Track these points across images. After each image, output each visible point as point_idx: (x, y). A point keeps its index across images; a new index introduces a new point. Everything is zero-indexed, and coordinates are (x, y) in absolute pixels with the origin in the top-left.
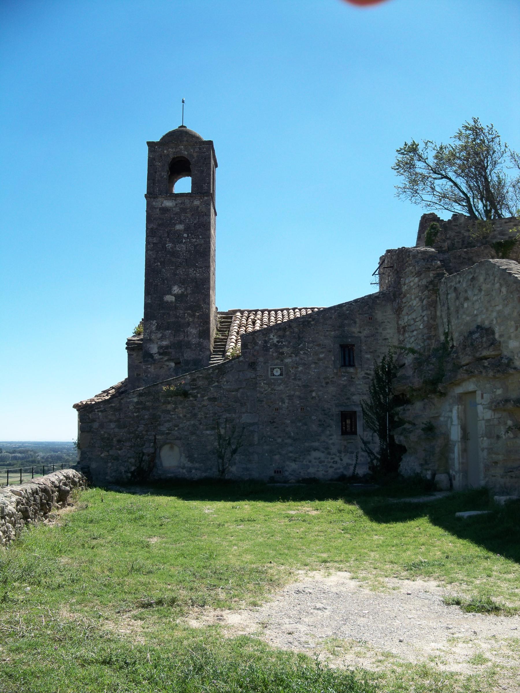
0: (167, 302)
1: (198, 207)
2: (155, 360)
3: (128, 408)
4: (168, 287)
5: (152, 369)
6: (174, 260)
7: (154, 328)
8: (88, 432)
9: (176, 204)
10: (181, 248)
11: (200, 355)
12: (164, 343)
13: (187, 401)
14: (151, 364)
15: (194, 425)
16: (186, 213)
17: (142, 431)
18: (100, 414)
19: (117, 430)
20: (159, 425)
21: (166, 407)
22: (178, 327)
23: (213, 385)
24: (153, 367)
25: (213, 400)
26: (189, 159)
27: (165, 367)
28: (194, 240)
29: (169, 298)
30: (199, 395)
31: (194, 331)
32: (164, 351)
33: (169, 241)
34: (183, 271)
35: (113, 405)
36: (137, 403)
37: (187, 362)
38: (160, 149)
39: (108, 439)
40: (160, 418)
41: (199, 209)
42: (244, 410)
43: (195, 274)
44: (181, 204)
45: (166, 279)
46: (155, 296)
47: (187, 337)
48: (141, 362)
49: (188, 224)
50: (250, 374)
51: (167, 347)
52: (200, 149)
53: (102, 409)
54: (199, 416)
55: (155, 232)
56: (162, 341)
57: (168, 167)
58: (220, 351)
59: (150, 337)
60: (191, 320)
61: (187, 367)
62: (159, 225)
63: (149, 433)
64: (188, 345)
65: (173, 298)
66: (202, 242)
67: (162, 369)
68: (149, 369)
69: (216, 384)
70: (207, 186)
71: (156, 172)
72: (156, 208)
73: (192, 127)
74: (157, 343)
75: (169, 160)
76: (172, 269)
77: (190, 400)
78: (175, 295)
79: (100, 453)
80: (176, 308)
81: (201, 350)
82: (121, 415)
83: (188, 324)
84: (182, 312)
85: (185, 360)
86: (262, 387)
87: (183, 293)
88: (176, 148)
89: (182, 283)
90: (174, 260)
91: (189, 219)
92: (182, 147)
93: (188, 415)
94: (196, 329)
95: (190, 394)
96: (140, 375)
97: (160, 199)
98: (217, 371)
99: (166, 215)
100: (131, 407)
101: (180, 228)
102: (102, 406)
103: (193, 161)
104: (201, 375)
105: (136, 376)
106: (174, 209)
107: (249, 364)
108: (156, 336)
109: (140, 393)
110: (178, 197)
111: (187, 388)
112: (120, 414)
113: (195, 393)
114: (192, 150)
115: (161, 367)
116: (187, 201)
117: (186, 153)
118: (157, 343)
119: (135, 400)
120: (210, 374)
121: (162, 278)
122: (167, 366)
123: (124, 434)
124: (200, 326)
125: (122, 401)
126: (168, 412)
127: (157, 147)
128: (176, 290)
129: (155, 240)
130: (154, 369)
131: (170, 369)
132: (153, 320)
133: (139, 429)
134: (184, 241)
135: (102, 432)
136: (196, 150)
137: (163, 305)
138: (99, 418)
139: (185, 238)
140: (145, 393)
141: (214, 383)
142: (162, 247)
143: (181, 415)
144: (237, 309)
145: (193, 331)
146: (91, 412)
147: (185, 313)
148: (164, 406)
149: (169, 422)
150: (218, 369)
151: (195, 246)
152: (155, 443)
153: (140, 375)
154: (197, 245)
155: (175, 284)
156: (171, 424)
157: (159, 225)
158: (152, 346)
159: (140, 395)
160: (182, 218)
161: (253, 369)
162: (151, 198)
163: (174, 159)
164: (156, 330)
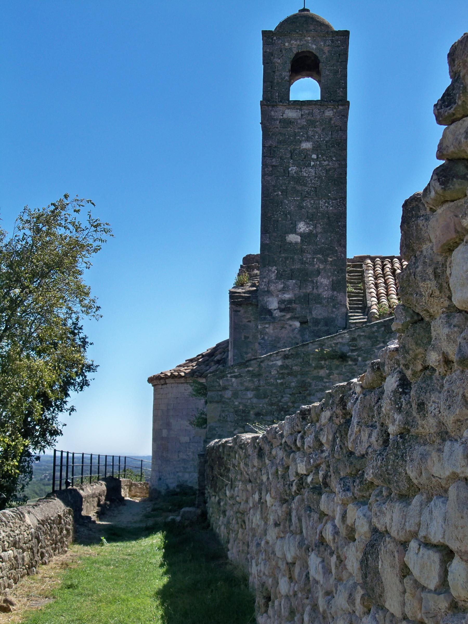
0: (291, 243)
1: (331, 119)
2: (274, 318)
3: (271, 373)
4: (292, 223)
5: (270, 329)
6: (299, 188)
7: (273, 276)
8: (217, 402)
9: (302, 115)
10: (309, 173)
11: (333, 312)
12: (287, 296)
13: (345, 366)
14: (269, 323)
16: (315, 127)
17: (287, 402)
18: (234, 380)
19: (255, 400)
20: (310, 395)
21: (318, 372)
22: (304, 276)
24: (271, 327)
26: (317, 55)
28: (326, 163)
29: (293, 238)
30: (360, 359)
32: (286, 307)
33: (293, 164)
34: (311, 203)
35: (251, 369)
36: (282, 367)
37: (316, 322)
38: (280, 41)
39: (244, 411)
40: (310, 386)
41: (332, 122)
43: (327, 207)
44: (309, 114)
45: (289, 213)
47: (317, 289)
49: (317, 142)
51: (290, 301)
52: (332, 42)
53: (237, 374)
55: (274, 151)
56: (284, 293)
57: (290, 65)
58: (358, 308)
59: (268, 287)
60: (321, 266)
61: (316, 328)
64: (318, 299)
67: (283, 330)
68: (267, 330)
70: (342, 91)
72: (275, 120)
73: (314, 11)
74: (277, 296)
75: (292, 56)
76: (297, 200)
77: (350, 365)
78: (301, 235)
79: (232, 429)
80: (302, 251)
81: (334, 306)
82: (261, 382)
83: (318, 272)
85: (313, 318)
87: (311, 232)
90: (299, 188)
91: (319, 136)
92: (309, 38)
94: (328, 278)
95: (349, 357)
96: (248, 337)
97: (280, 108)
98: (383, 329)
99: (289, 129)
100: (274, 372)
101: (307, 147)
102: (236, 370)
103: (323, 58)
104: (363, 334)
105: (243, 339)
106: (299, 121)
108: (276, 287)
109: (285, 355)
111: (345, 349)
112: (259, 381)
113: (355, 356)
114: (322, 43)
115: (282, 328)
116: (316, 111)
117: (314, 47)
118: (277, 296)
119: (279, 363)
120: (374, 333)
121: (283, 212)
122: (291, 326)
123: (265, 405)
124: (333, 274)
125: (262, 365)
126: (321, 379)
127: (275, 38)
128: (302, 227)
130: (273, 330)
131: (293, 330)
133: (283, 400)
134: (312, 163)
135: (237, 403)
138: (232, 385)
139: (313, 160)
140: (292, 354)
141: (379, 344)
142: (284, 170)
144: (366, 255)
145: (324, 281)
146: (222, 378)
147: (314, 258)
148: (315, 372)
150: (385, 326)
153: (248, 337)
154: (330, 170)
155: (301, 220)
158: (270, 299)
159: (286, 357)
160: (310, 133)
163: (298, 54)
164: (276, 279)
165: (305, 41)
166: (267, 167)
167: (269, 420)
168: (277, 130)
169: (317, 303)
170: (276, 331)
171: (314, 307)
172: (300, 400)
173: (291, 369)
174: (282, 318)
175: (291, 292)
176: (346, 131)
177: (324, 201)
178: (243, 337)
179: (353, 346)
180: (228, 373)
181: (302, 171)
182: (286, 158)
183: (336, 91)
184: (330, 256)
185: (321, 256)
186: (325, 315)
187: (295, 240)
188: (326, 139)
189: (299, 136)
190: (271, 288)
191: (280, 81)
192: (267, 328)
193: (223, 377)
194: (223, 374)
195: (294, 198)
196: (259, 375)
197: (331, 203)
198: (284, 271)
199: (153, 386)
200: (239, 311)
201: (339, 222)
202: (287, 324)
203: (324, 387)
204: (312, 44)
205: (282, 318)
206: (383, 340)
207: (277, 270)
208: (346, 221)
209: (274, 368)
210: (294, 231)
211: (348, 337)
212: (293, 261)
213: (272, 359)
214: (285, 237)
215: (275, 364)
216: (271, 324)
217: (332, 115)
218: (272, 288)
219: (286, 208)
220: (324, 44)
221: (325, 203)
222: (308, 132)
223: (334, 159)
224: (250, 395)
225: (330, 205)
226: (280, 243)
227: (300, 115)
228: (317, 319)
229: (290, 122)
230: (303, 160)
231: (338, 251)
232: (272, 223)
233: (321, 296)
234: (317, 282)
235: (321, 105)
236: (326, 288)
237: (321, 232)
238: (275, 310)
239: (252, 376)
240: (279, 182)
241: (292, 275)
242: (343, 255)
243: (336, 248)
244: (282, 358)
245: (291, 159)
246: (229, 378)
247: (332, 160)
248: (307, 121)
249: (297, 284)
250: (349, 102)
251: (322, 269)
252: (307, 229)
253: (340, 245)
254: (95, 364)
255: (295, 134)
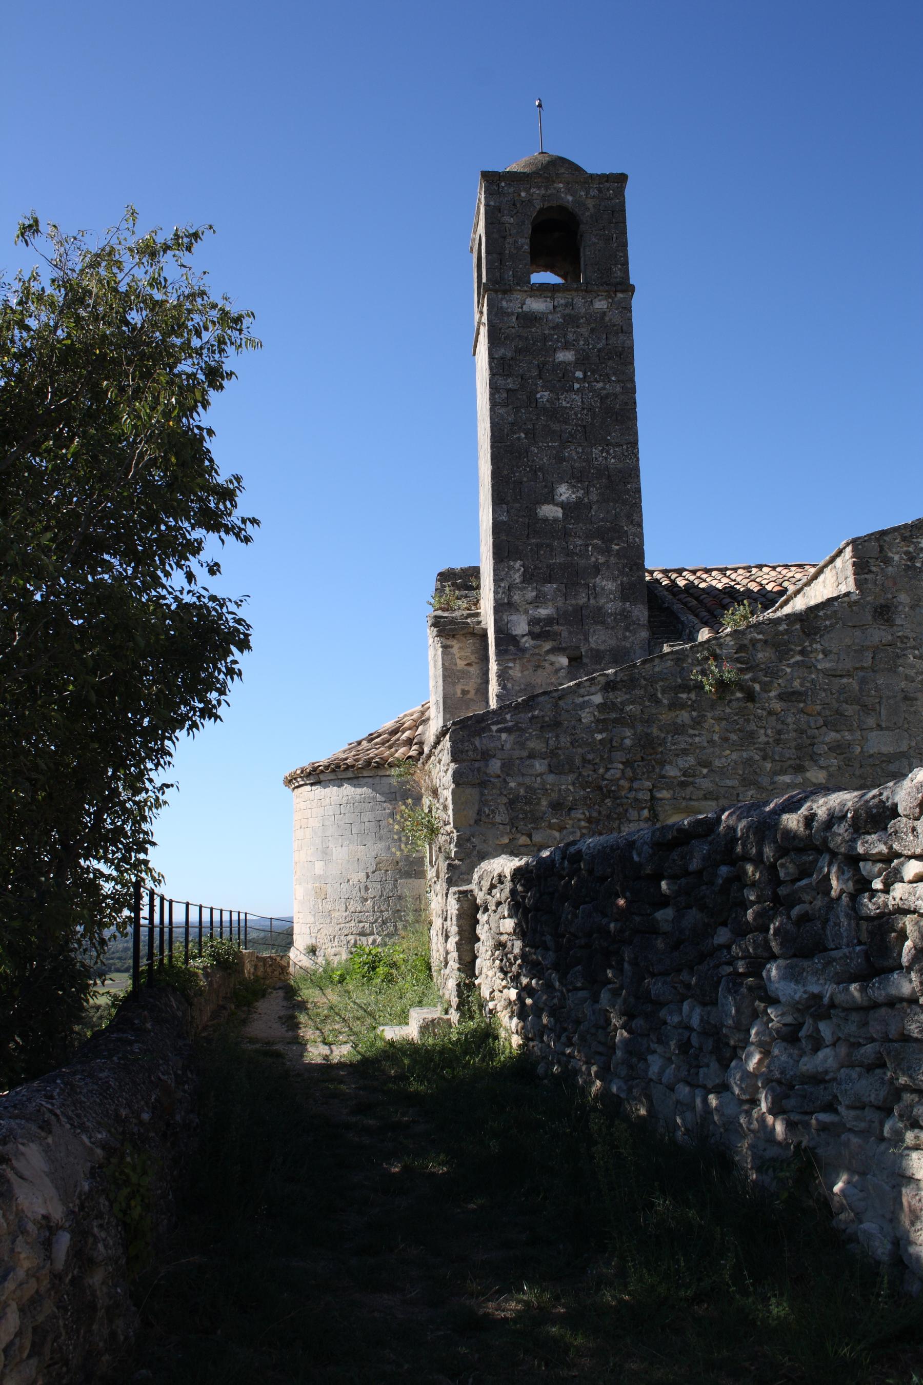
0: (545, 520)
1: (604, 313)
2: (523, 650)
3: (580, 720)
4: (546, 486)
6: (556, 427)
7: (517, 577)
9: (555, 307)
10: (571, 401)
12: (543, 612)
14: (514, 660)
15: (749, 762)
16: (578, 327)
18: (504, 736)
19: (551, 778)
23: (793, 660)
25: (787, 696)
27: (546, 665)
28: (600, 385)
29: (550, 511)
31: (610, 585)
33: (542, 387)
34: (578, 453)
36: (602, 707)
38: (512, 189)
41: (607, 319)
42: (871, 722)
43: (606, 458)
44: (566, 306)
45: (541, 469)
46: (517, 505)
47: (595, 598)
48: (469, 664)
50: (879, 635)
51: (549, 621)
52: (600, 191)
53: (510, 724)
54: (763, 739)
55: (510, 366)
56: (538, 607)
57: (530, 226)
59: (510, 597)
60: (602, 560)
62: (518, 351)
63: (636, 785)
64: (599, 616)
65: (558, 512)
66: (618, 389)
67: (540, 671)
68: (511, 672)
69: (798, 658)
70: (620, 270)
71: (505, 238)
74: (526, 612)
78: (562, 505)
80: (566, 534)
82: (562, 740)
84: (579, 542)
85: (592, 649)
86: (912, 666)
88: (546, 188)
89: (577, 478)
90: (556, 427)
91: (586, 340)
92: (561, 185)
93: (734, 737)
94: (615, 580)
96: (468, 692)
97: (517, 296)
99: (533, 330)
101: (566, 359)
102: (508, 717)
104: (761, 637)
105: (459, 694)
106: (550, 317)
107: (876, 611)
110: (558, 291)
112: (557, 737)
113: (747, 681)
114: (583, 193)
117: (570, 198)
118: (526, 612)
119: (598, 699)
122: (552, 664)
123: (571, 787)
125: (561, 703)
126: (678, 729)
127: (503, 184)
128: (564, 492)
129: (511, 383)
132: (515, 560)
134: (576, 386)
135: (512, 784)
136: (592, 194)
137: (536, 526)
139: (578, 380)
140: (622, 681)
141: (793, 657)
142: (529, 398)
143: (716, 737)
147: (588, 545)
149: (687, 755)
151: (603, 399)
152: (652, 809)
154: (607, 396)
155: (561, 480)
156: (691, 760)
157: (518, 351)
158: (514, 618)
159: (610, 686)
160: (570, 336)
161: (887, 621)
162: (496, 291)
163: (541, 211)
164: (523, 582)
165: (555, 188)
166: (499, 392)
167: (582, 817)
168: (513, 331)
169: (596, 623)
170: (526, 673)
171: (591, 631)
172: (644, 773)
173: (622, 710)
174: (537, 651)
175: (550, 604)
176: (631, 332)
177: (600, 448)
178: (459, 692)
179: (741, 663)
180: (493, 724)
181: (559, 399)
182: (531, 377)
183: (611, 269)
184: (616, 542)
185: (600, 542)
186: (613, 642)
187: (552, 515)
188: (598, 346)
189: (551, 341)
190: (515, 597)
191: (515, 252)
192: (510, 668)
193: (483, 730)
194: (483, 725)
195: (548, 443)
196: (556, 724)
197: (611, 451)
198: (536, 568)
199: (442, 647)
200: (452, 647)
201: (628, 483)
202: (545, 660)
203: (691, 745)
204: (566, 194)
205: (537, 651)
206: (800, 648)
207: (523, 566)
208: (639, 481)
209: (587, 710)
210: (550, 498)
211: (732, 643)
212: (552, 550)
213: (582, 691)
214: (536, 509)
215: (588, 701)
216: (518, 662)
217: (605, 306)
218: (516, 598)
219: (534, 460)
220: (586, 195)
221: (602, 452)
222: (566, 334)
223: (613, 378)
224: (539, 766)
225: (610, 455)
226: (527, 520)
227: (551, 307)
228: (598, 650)
229: (536, 318)
230: (560, 381)
231: (629, 533)
232: (512, 486)
233: (603, 611)
234: (594, 586)
235: (586, 291)
236: (612, 596)
237: (597, 501)
238: (523, 636)
239: (542, 727)
240: (520, 417)
241: (550, 576)
242: (637, 540)
243: (625, 528)
244: (601, 690)
245: (541, 378)
246: (495, 734)
247: (610, 381)
248: (564, 317)
249: (560, 591)
250: (633, 286)
251: (603, 564)
252: (574, 496)
253: (632, 523)
254: (244, 506)
255: (545, 338)
